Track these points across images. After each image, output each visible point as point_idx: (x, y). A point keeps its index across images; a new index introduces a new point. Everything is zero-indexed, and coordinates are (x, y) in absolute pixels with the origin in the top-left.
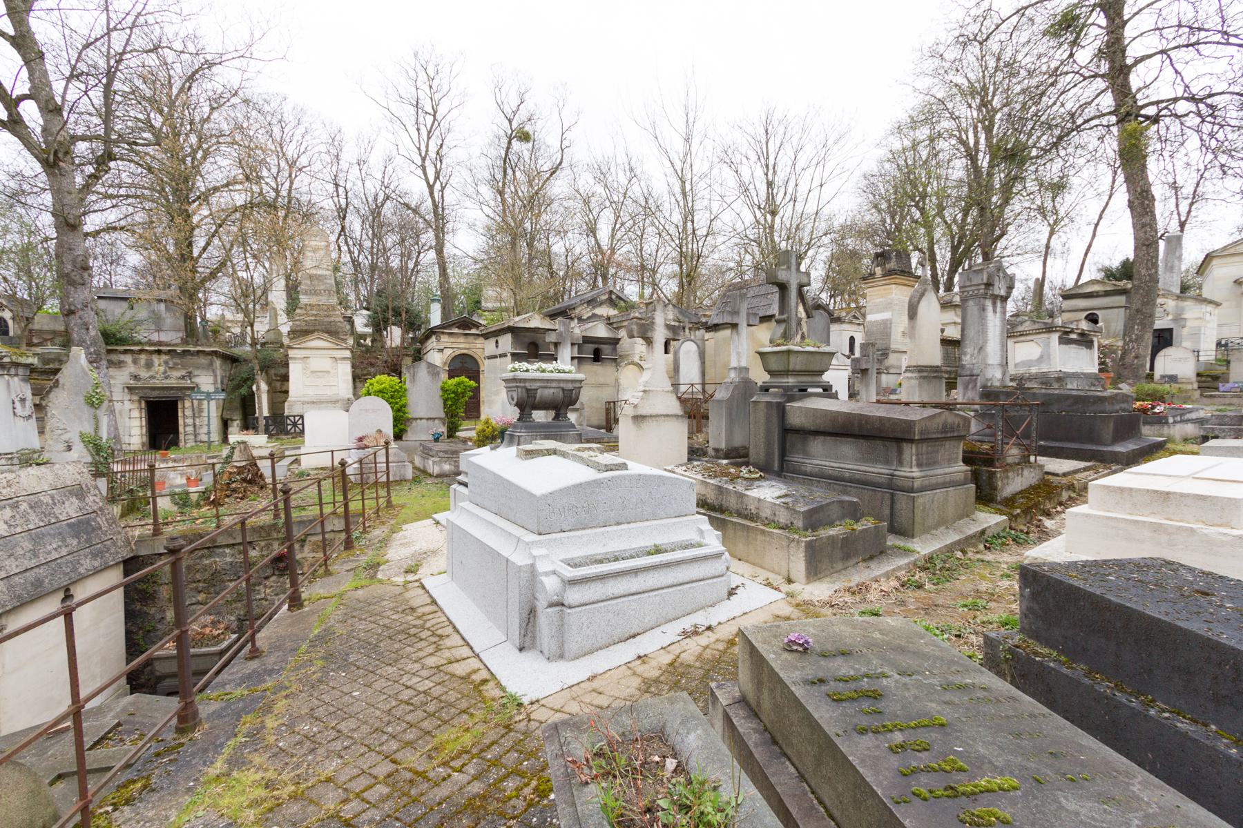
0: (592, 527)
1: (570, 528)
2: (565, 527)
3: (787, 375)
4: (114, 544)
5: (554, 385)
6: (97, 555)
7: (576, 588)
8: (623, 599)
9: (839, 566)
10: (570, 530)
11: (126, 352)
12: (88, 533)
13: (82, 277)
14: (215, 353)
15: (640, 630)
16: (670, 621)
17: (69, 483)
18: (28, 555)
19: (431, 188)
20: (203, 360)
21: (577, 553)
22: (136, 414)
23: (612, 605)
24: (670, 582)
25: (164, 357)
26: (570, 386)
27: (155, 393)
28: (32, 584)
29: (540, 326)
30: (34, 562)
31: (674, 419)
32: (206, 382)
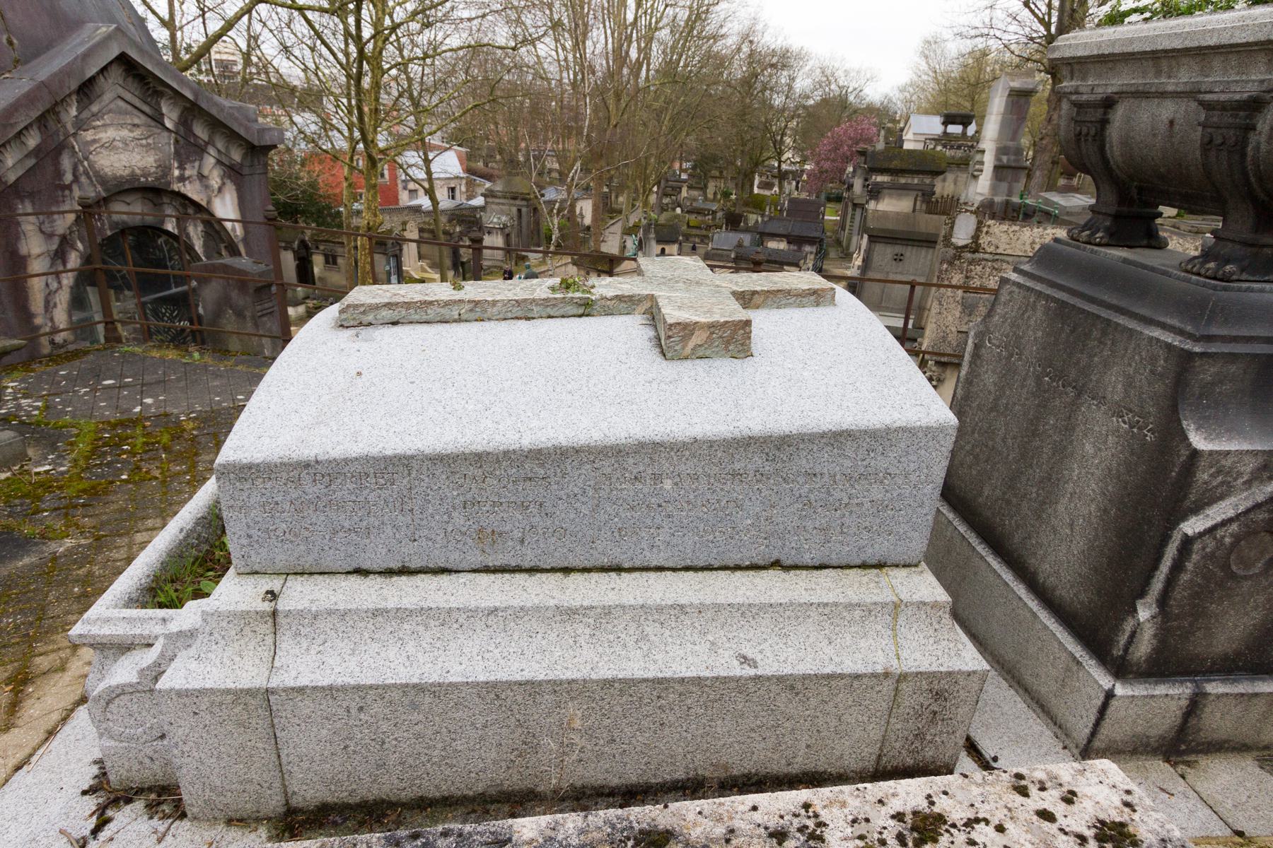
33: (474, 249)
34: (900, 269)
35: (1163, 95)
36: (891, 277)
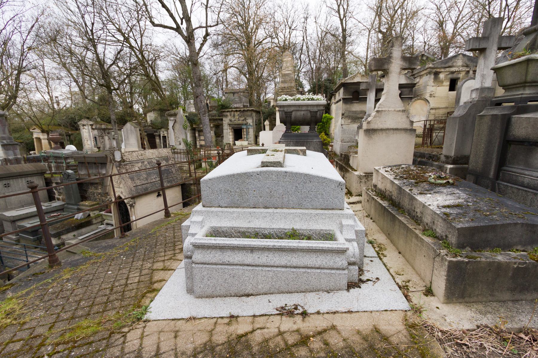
0: (244, 207)
1: (226, 205)
2: (221, 204)
3: (524, 87)
4: (177, 178)
5: (304, 108)
6: (169, 182)
7: (200, 251)
8: (238, 267)
9: (507, 296)
10: (226, 207)
11: (228, 111)
12: (167, 174)
13: (199, 83)
14: (252, 110)
15: (254, 293)
16: (283, 292)
17: (163, 156)
18: (144, 179)
19: (341, 20)
20: (249, 113)
21: (225, 223)
22: (231, 134)
23: (228, 269)
24: (283, 263)
25: (238, 113)
26: (315, 109)
27: (236, 126)
28: (144, 189)
29: (361, 81)
30: (146, 182)
31: (403, 132)
32: (250, 121)
33: (33, 193)
34: (10, 190)
35: (301, 111)
36: (7, 194)
